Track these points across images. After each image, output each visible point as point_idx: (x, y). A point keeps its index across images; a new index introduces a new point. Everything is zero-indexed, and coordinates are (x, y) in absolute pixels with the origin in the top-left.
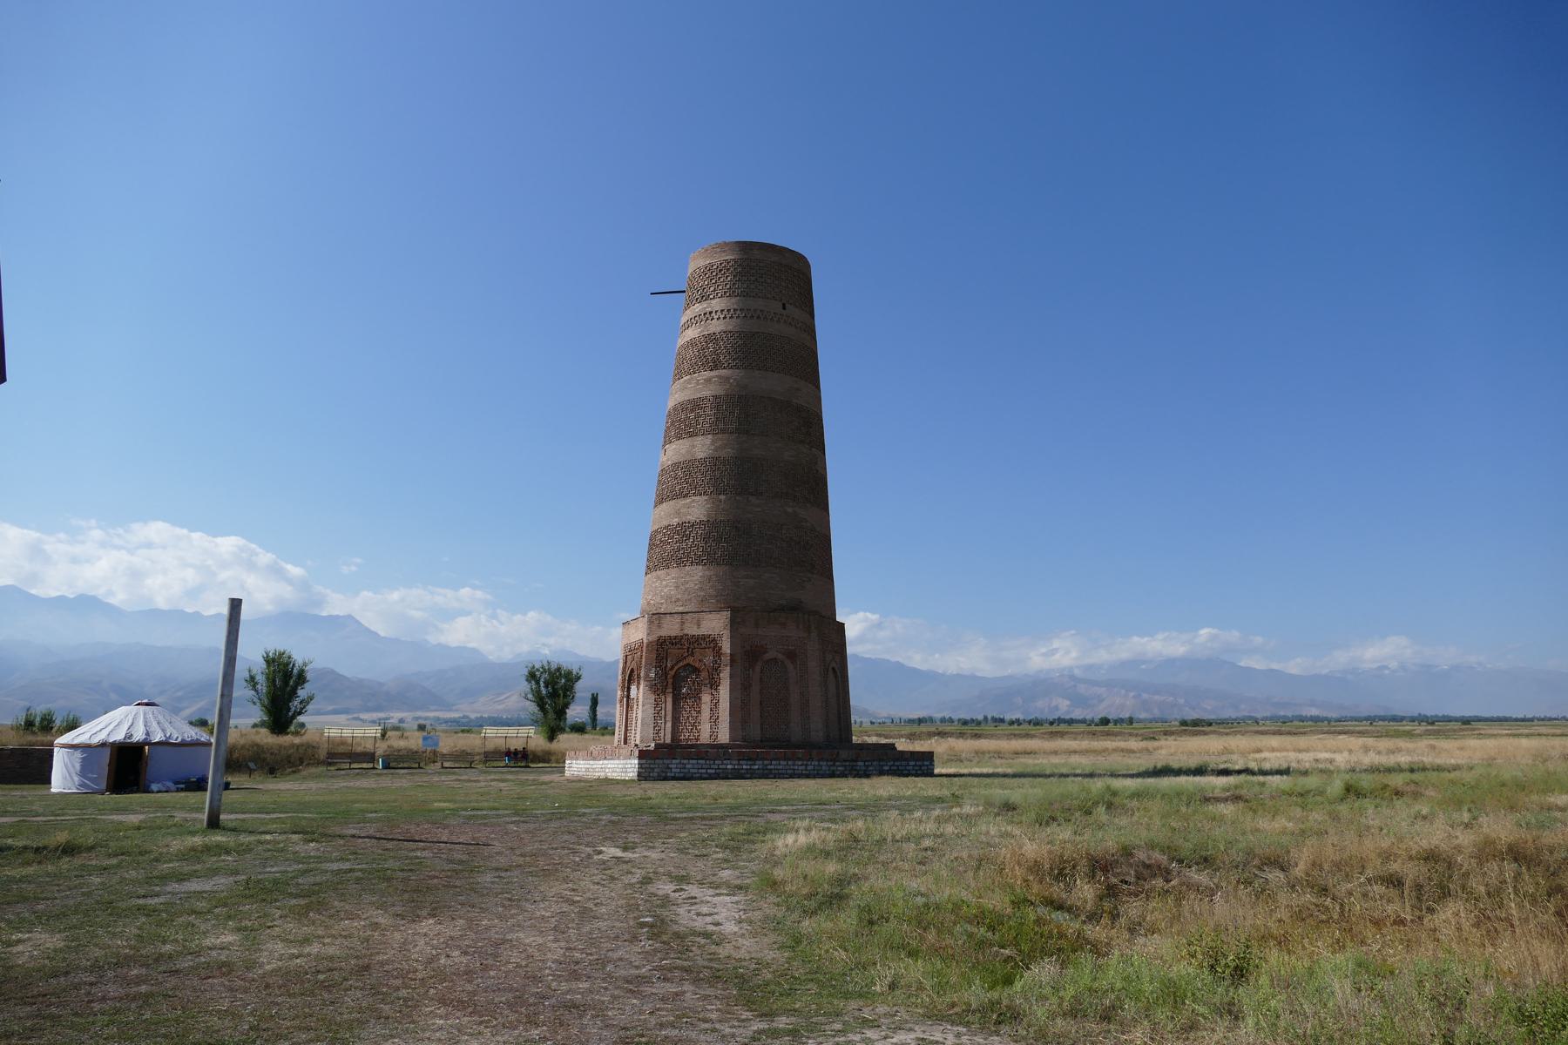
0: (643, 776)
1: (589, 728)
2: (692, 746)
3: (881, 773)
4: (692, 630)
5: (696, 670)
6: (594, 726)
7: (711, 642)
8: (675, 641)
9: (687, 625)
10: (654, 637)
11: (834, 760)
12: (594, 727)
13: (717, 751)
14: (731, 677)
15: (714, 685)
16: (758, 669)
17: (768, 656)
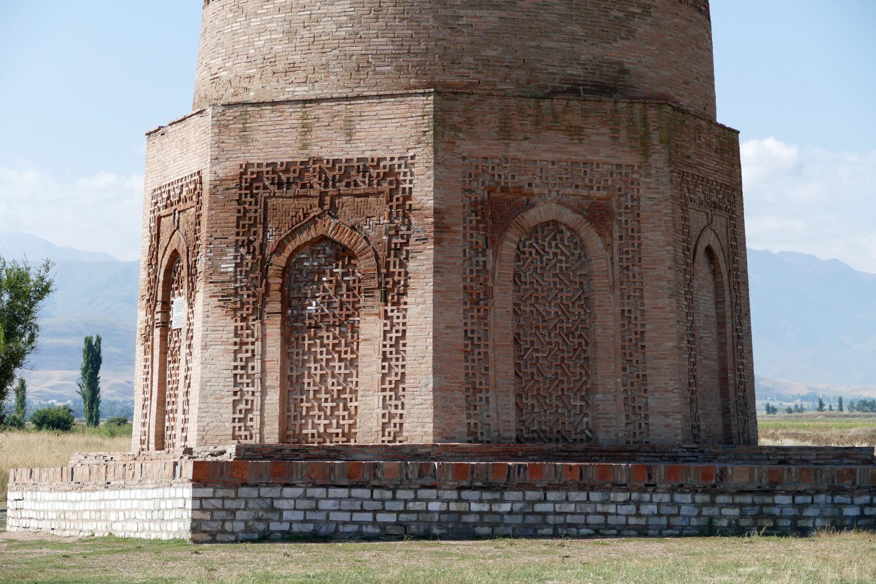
0: (207, 531)
1: (80, 420)
2: (335, 453)
3: (839, 525)
4: (331, 147)
5: (344, 254)
6: (89, 412)
7: (381, 179)
8: (286, 177)
9: (319, 132)
10: (230, 168)
11: (713, 491)
12: (94, 419)
13: (401, 464)
14: (438, 269)
15: (392, 291)
16: (508, 248)
17: (534, 216)
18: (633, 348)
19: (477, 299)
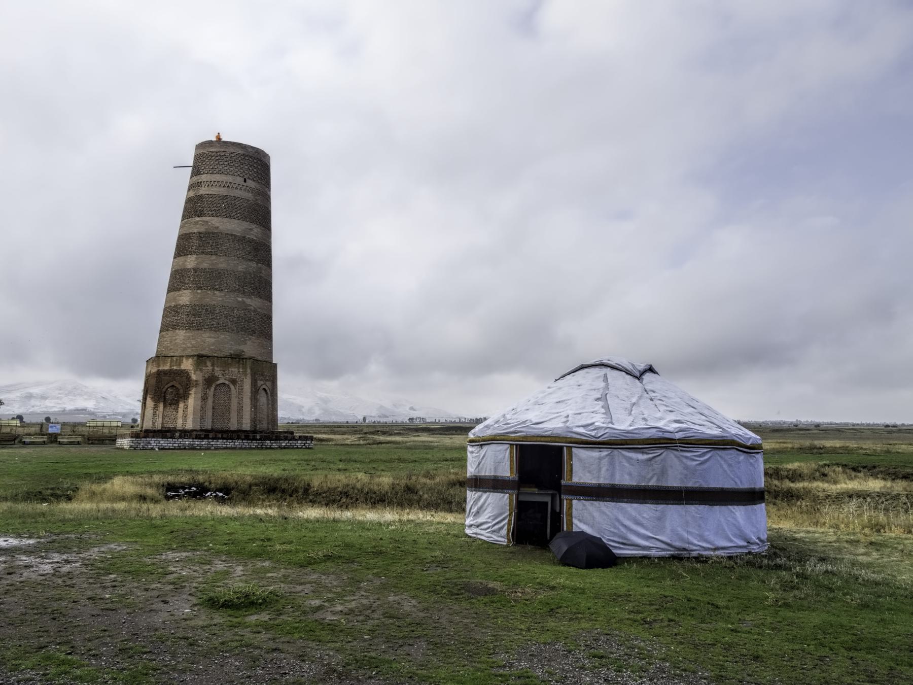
16: (212, 389)
18: (240, 410)
19: (204, 399)
